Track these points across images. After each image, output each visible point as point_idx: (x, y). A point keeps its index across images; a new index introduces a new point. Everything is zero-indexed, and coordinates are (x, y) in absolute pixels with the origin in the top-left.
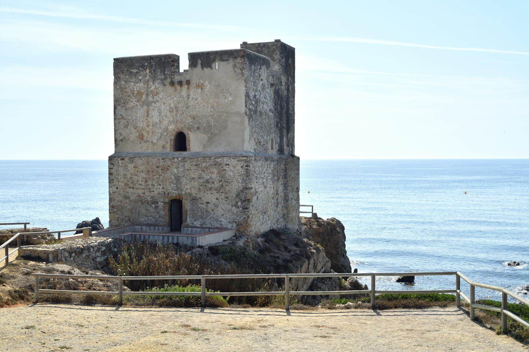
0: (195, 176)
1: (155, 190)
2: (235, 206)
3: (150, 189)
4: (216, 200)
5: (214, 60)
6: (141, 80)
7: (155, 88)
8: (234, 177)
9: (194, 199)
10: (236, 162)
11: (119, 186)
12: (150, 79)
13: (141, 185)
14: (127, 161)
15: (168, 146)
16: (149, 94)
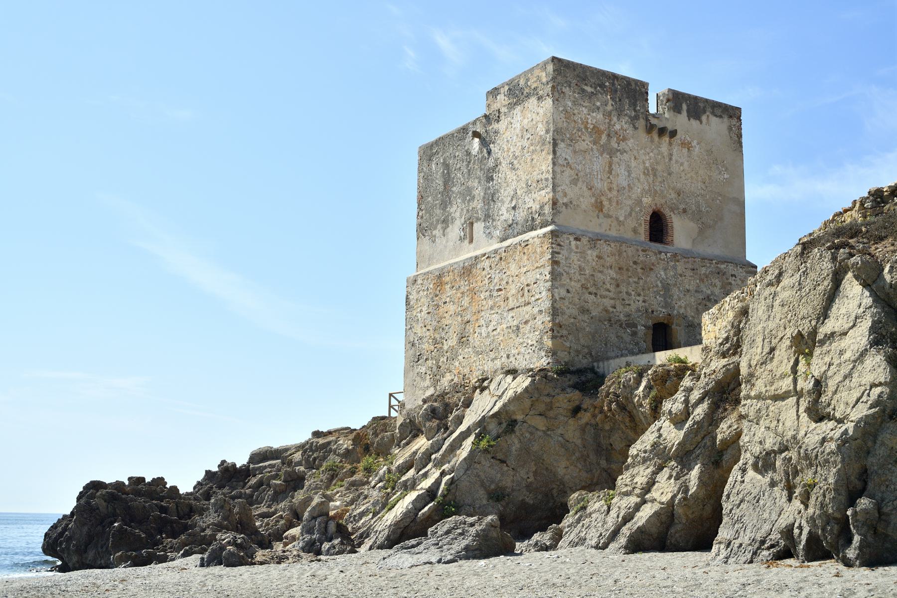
3: (623, 300)
6: (598, 108)
9: (691, 326)
14: (585, 243)
16: (611, 135)
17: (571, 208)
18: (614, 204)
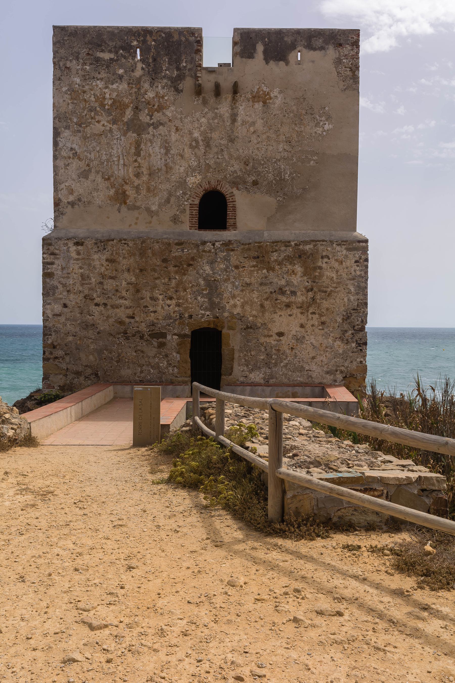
0: (253, 278)
3: (146, 307)
4: (299, 329)
5: (293, 47)
6: (121, 77)
7: (156, 96)
9: (251, 328)
10: (344, 252)
12: (144, 75)
15: (186, 218)
18: (144, 192)
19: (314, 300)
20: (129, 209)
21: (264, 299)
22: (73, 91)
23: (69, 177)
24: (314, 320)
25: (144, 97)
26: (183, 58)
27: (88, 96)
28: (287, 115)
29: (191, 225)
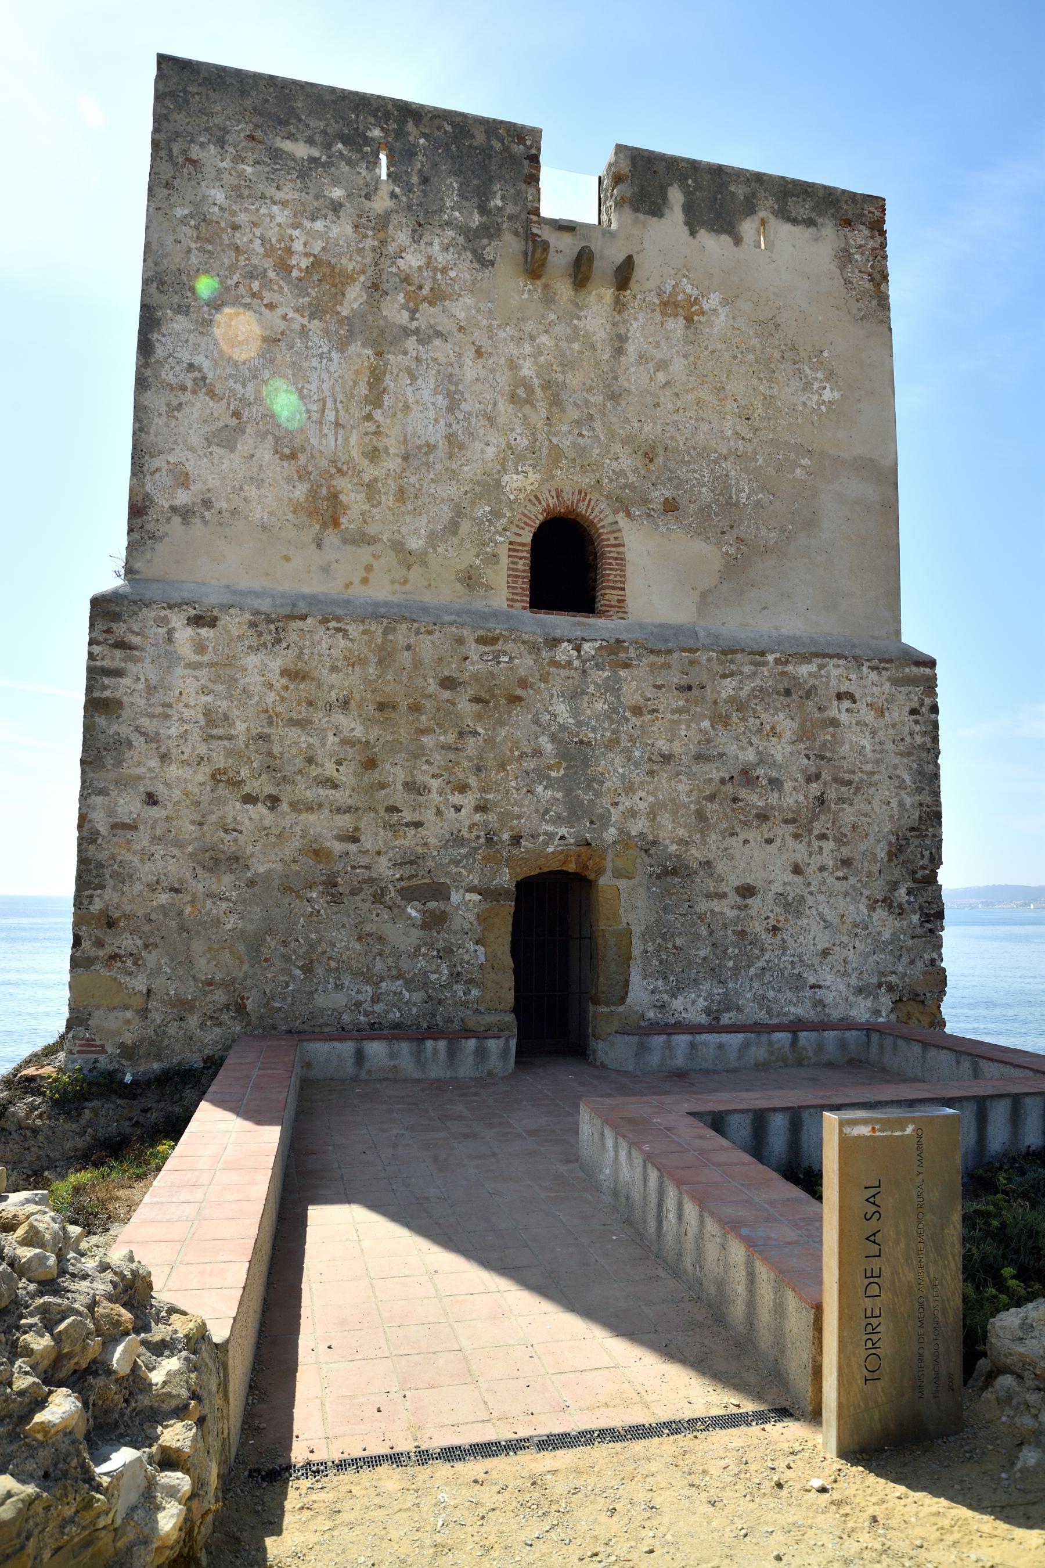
0: (677, 743)
1: (429, 816)
2: (888, 902)
3: (393, 809)
4: (789, 877)
5: (750, 208)
6: (336, 207)
8: (877, 762)
9: (674, 872)
10: (887, 686)
11: (167, 784)
13: (332, 784)
14: (235, 632)
16: (385, 286)
17: (205, 522)
18: (388, 500)
19: (823, 803)
20: (345, 541)
21: (705, 798)
22: (204, 220)
23: (180, 441)
24: (825, 855)
25: (394, 263)
26: (495, 189)
27: (245, 240)
28: (739, 356)
29: (511, 597)
